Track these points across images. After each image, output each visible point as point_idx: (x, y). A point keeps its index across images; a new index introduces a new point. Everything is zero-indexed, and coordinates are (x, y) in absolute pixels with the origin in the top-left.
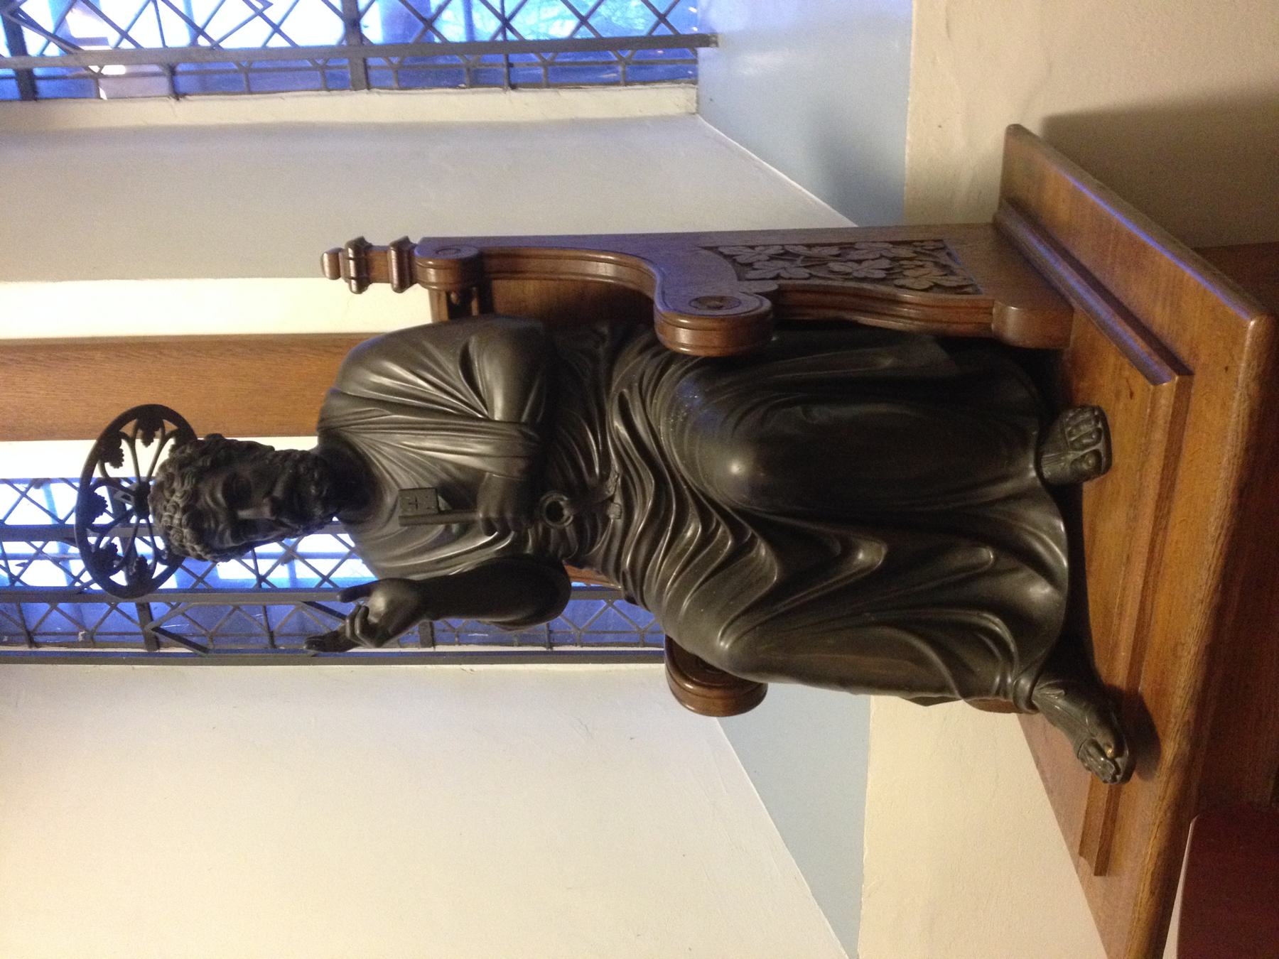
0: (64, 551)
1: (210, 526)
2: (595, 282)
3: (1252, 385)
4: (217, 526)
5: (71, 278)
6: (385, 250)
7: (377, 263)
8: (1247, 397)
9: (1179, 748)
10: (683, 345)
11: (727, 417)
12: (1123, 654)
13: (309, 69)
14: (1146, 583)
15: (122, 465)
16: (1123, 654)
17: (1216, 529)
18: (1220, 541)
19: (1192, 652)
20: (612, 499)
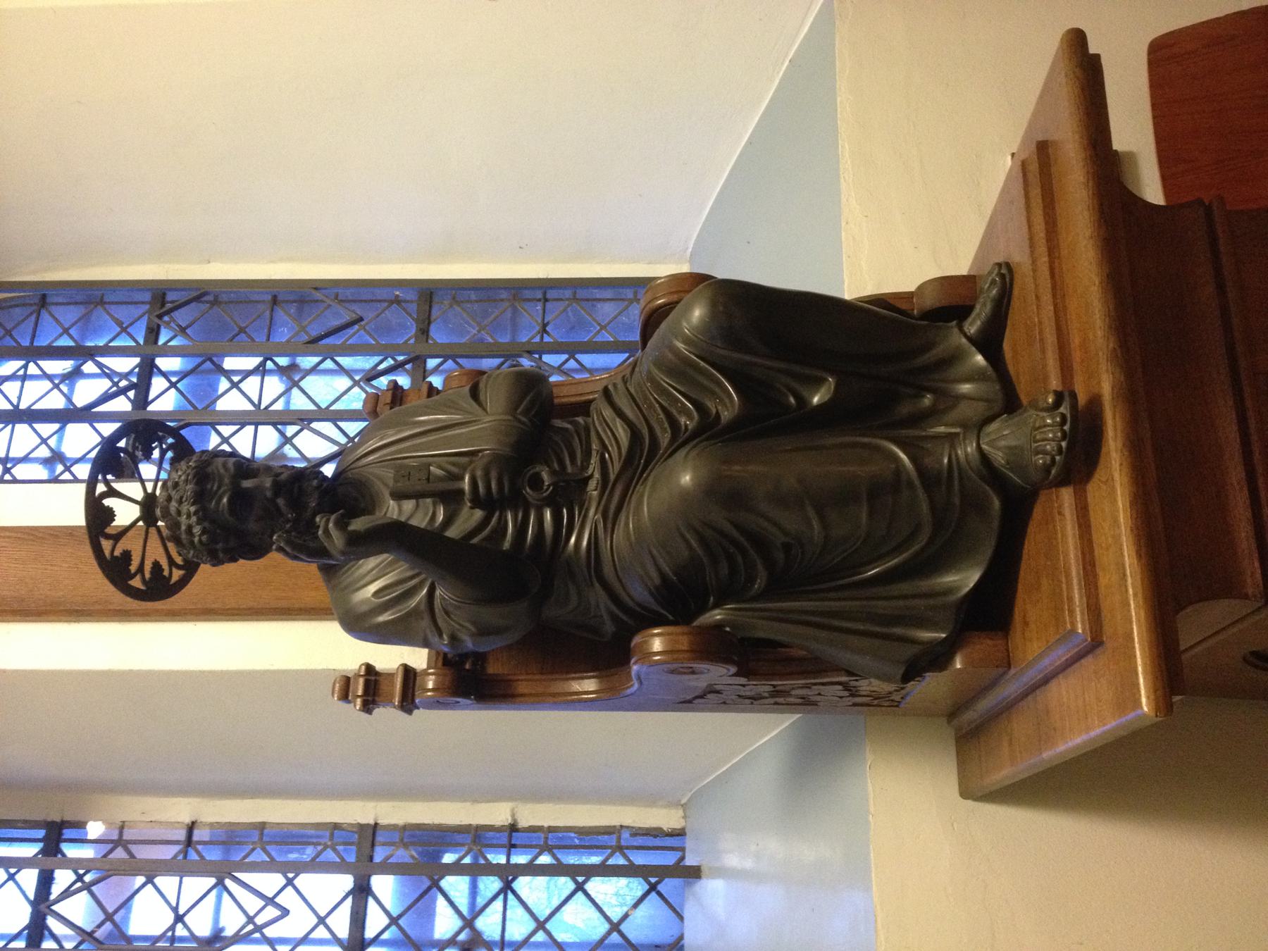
0: (118, 386)
1: (212, 487)
2: (581, 672)
3: (1077, 70)
4: (219, 488)
5: (241, 356)
6: (390, 676)
7: (384, 687)
8: (1076, 79)
9: (1113, 378)
10: (658, 635)
11: (687, 651)
12: (1055, 382)
13: (462, 356)
14: (1055, 306)
15: (124, 551)
16: (1055, 382)
17: (1084, 177)
18: (1090, 184)
19: (1097, 283)
20: (591, 476)
